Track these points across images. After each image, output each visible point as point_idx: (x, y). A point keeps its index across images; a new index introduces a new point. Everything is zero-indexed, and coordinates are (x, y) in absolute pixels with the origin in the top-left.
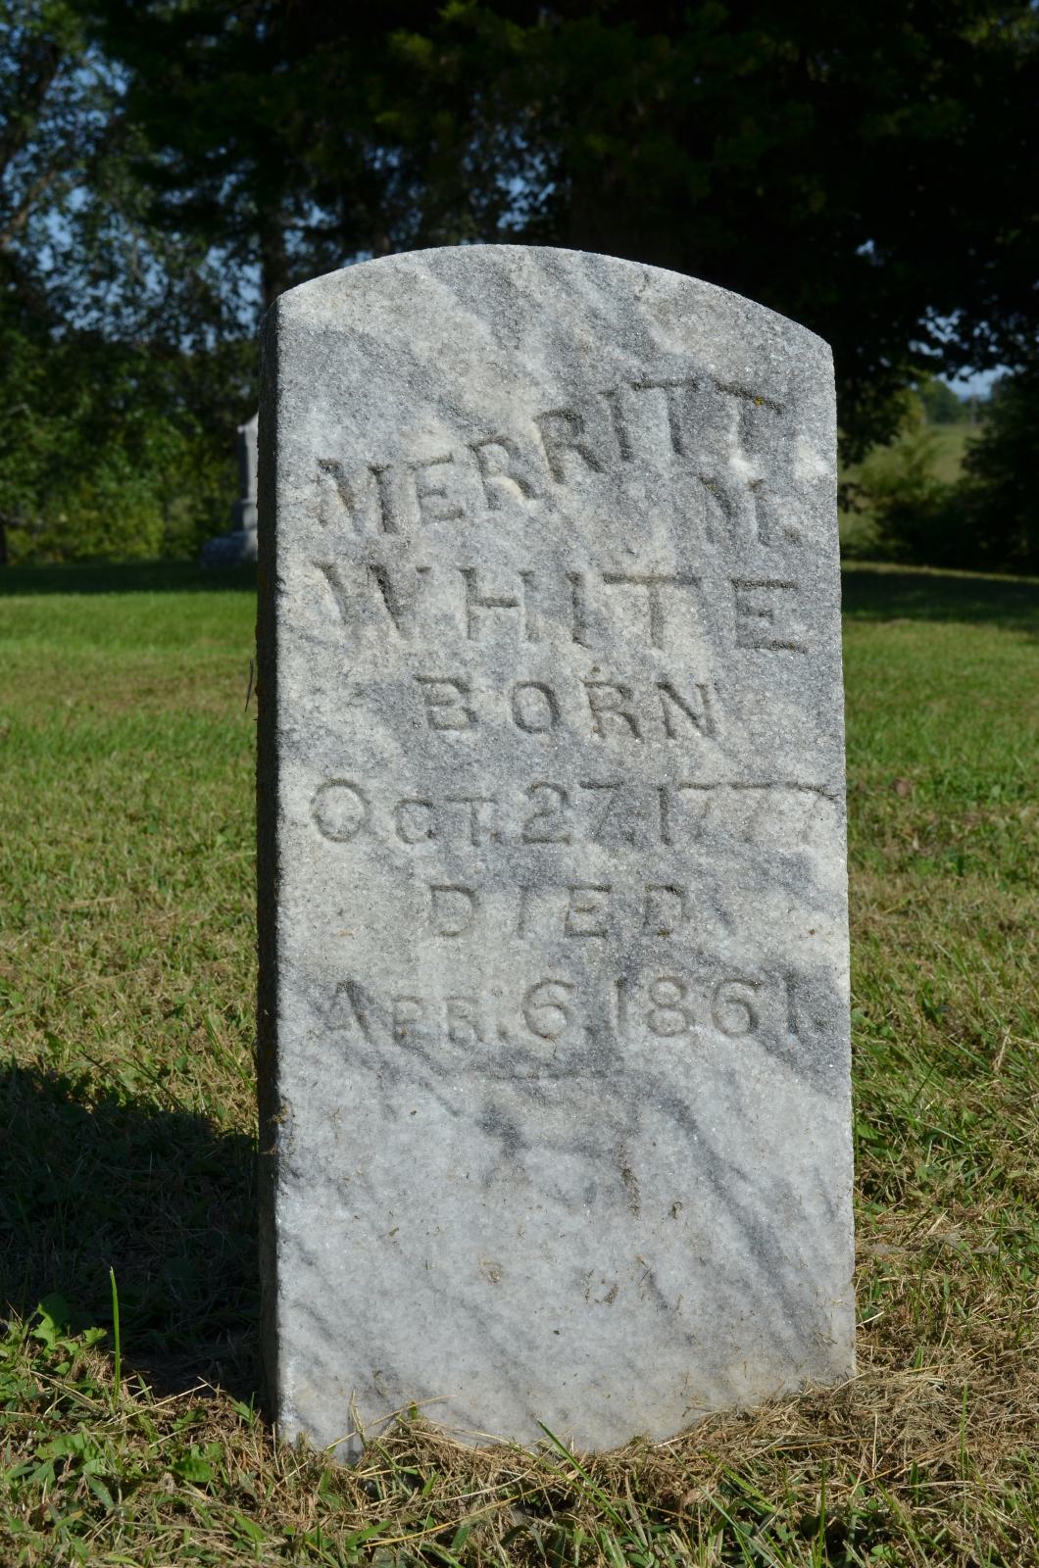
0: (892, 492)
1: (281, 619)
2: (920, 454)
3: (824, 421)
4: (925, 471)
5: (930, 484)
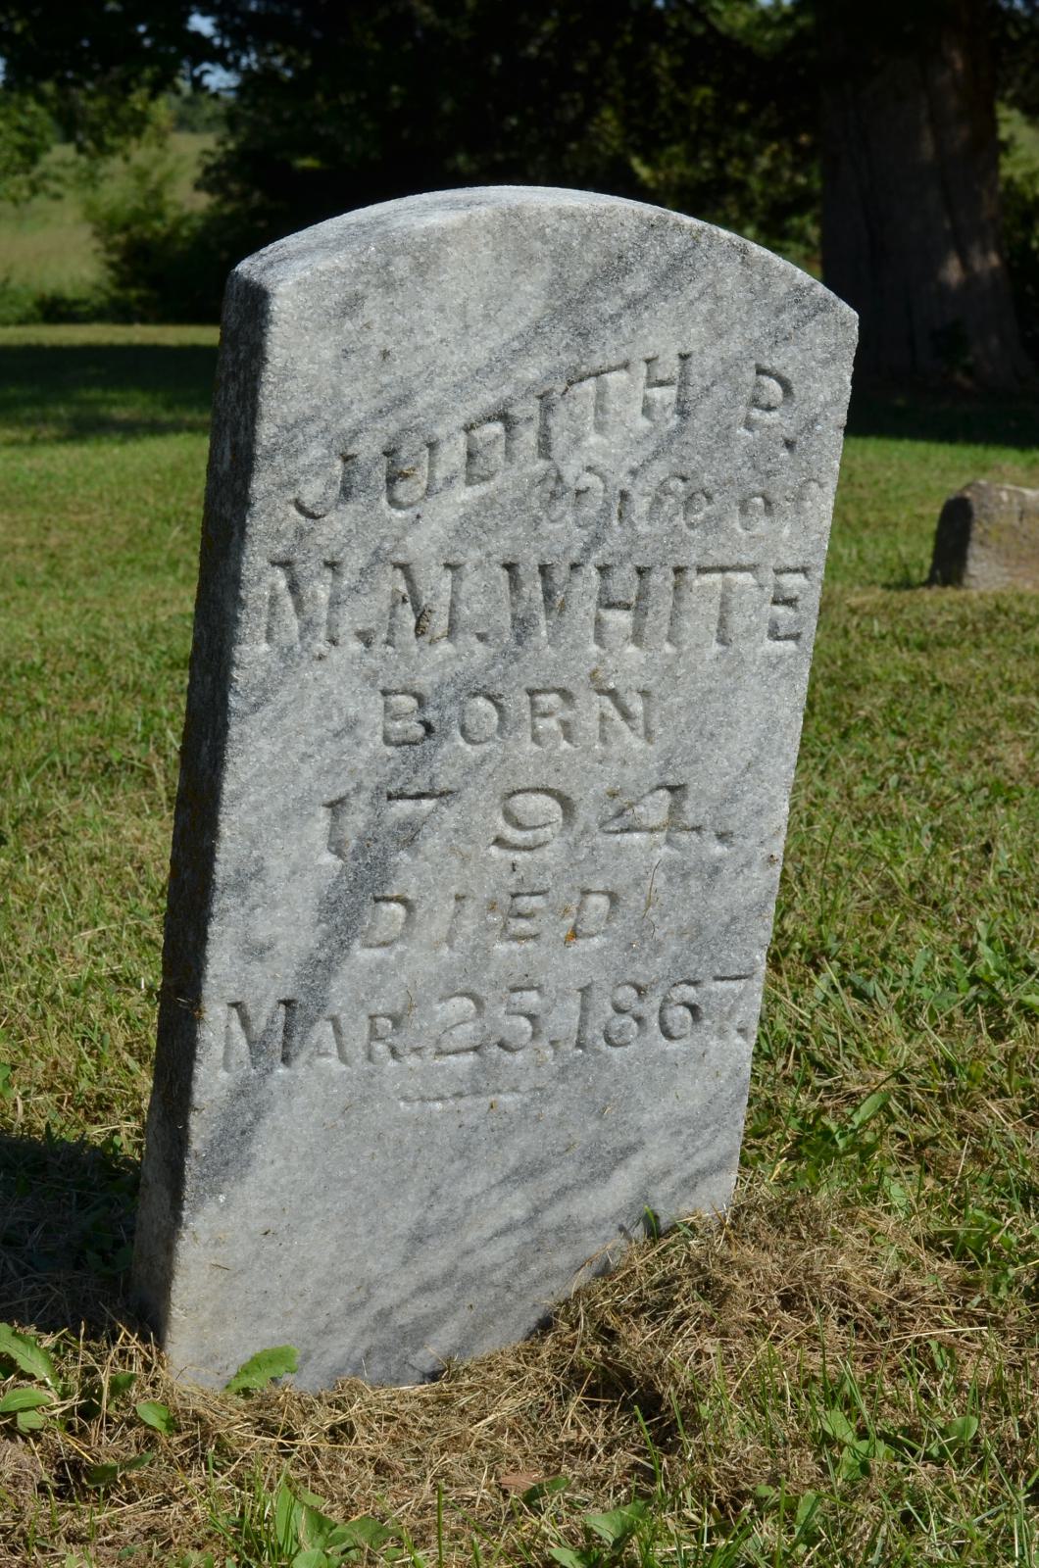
0: (126, 228)
1: (264, 409)
2: (155, 176)
3: (426, 256)
4: (168, 197)
5: (172, 213)
